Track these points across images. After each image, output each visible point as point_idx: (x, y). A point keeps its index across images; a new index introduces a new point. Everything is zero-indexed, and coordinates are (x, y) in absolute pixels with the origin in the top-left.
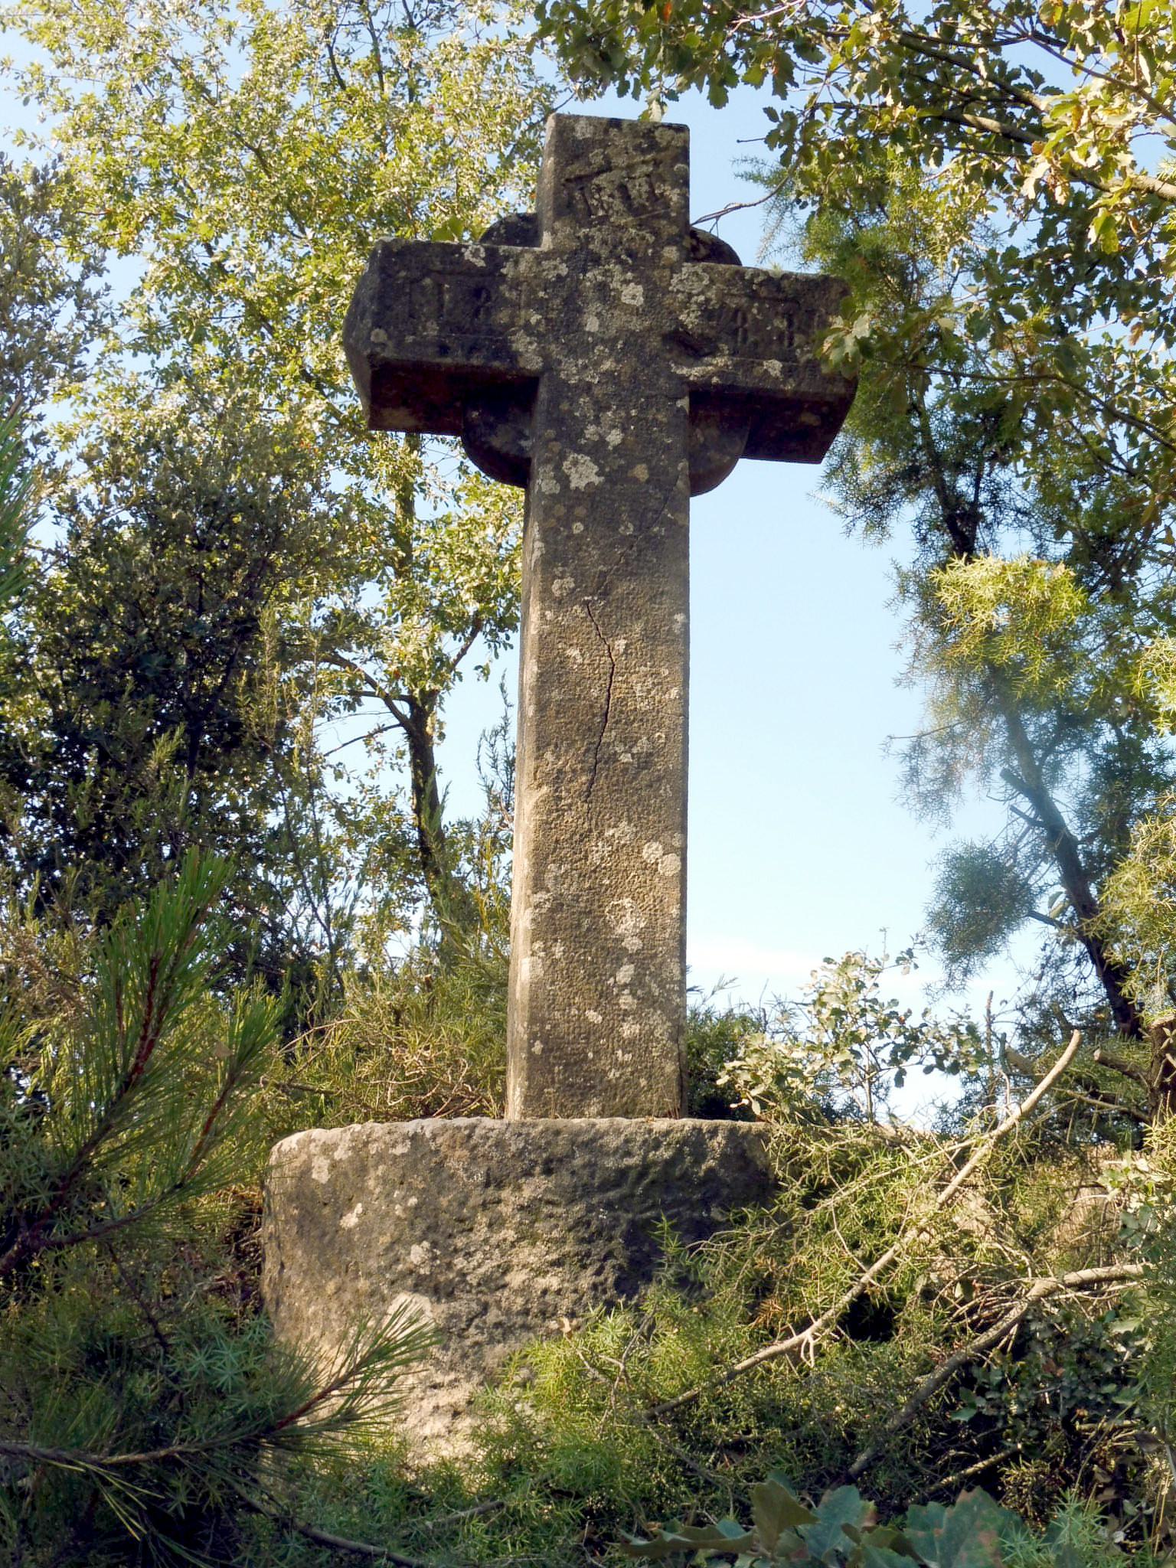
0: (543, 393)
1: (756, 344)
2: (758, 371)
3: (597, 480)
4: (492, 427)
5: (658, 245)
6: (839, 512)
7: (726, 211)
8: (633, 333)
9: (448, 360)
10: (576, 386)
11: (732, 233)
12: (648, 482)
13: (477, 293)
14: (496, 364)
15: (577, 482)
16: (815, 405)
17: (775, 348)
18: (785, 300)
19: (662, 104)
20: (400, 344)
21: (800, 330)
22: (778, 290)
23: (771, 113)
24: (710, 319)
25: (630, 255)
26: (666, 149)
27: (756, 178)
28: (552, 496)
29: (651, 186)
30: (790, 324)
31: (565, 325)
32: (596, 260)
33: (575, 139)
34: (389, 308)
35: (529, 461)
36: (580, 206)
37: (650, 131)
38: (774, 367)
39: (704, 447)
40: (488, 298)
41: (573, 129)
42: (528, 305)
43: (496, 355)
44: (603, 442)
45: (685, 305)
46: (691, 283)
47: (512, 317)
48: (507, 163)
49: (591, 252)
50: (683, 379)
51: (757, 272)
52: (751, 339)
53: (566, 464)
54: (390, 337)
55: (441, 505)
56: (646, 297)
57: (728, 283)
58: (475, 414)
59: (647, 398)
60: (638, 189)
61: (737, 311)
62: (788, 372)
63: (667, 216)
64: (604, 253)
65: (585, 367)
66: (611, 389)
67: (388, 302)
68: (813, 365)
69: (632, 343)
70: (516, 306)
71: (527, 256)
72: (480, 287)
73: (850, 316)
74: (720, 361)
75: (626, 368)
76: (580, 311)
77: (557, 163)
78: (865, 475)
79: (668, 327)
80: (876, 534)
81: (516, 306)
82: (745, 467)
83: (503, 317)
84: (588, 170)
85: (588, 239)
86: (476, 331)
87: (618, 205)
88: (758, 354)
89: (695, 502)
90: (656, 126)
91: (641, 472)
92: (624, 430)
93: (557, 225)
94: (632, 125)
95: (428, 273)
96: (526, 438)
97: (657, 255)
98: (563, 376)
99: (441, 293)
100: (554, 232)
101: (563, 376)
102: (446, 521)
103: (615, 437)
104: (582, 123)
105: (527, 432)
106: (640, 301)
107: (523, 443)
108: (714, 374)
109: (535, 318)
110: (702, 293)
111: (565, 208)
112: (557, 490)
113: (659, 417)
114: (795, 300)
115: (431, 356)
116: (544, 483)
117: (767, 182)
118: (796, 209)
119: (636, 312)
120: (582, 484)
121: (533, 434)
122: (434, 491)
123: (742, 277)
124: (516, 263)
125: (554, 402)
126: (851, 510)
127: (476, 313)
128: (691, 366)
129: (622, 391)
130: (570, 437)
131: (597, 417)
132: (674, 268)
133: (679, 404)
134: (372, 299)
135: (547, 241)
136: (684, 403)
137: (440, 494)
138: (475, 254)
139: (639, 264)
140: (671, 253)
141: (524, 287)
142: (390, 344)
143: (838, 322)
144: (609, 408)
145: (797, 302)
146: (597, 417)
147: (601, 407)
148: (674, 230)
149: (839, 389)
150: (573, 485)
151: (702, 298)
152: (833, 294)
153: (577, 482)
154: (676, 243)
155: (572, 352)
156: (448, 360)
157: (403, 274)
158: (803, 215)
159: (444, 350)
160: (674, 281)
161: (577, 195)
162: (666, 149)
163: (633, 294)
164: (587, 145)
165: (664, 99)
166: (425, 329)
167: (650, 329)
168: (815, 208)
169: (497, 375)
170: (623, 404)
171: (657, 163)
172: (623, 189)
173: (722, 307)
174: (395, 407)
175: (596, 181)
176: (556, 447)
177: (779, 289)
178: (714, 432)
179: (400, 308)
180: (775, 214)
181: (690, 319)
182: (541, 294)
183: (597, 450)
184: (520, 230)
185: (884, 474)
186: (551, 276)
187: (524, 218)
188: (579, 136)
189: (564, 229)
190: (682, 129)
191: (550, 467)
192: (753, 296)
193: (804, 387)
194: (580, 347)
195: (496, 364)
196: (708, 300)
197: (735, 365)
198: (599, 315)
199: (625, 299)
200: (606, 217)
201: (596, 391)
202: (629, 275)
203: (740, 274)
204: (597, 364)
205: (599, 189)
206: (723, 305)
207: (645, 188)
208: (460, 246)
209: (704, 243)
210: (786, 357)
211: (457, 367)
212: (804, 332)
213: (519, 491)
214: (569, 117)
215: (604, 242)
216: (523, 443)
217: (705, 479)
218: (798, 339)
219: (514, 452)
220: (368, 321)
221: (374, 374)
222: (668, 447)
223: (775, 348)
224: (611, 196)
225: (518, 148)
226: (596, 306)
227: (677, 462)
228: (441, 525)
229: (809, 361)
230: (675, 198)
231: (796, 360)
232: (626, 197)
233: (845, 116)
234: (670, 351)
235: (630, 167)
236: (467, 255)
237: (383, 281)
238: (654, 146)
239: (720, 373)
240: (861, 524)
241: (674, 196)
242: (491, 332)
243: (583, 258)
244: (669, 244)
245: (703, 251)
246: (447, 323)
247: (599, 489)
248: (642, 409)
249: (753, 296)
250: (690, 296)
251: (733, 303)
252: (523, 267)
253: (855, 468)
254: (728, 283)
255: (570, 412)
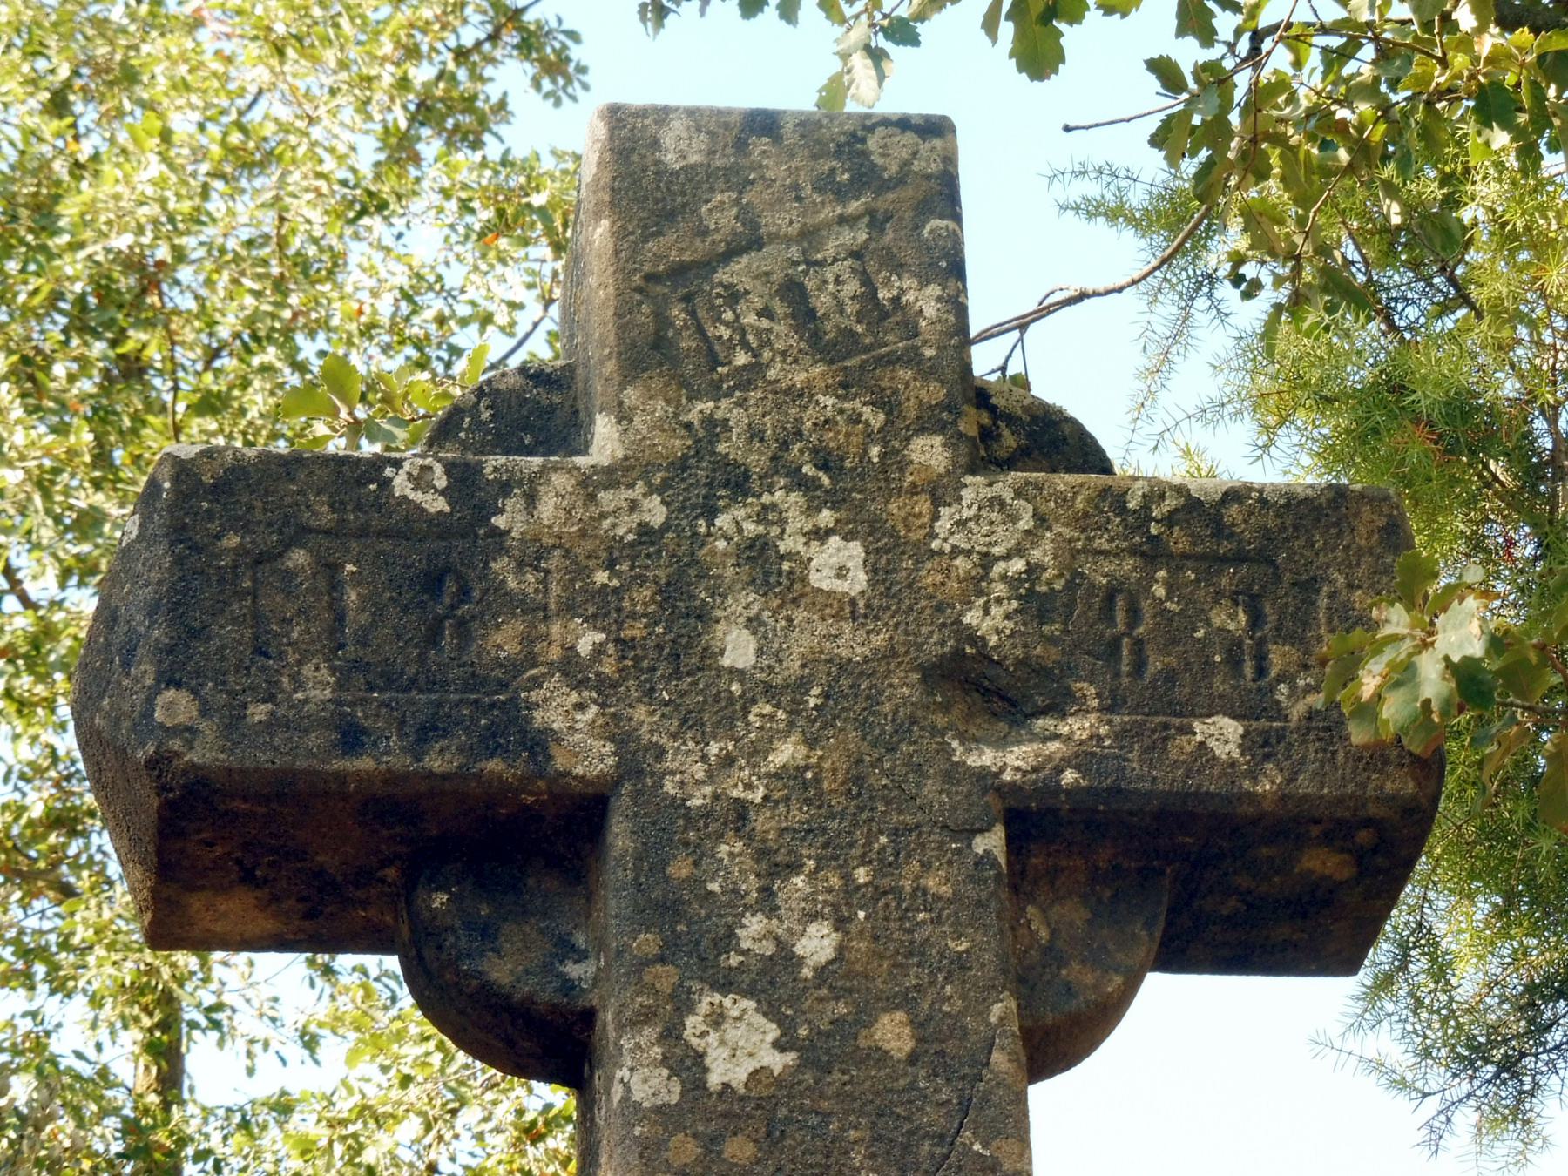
0: (621, 836)
1: (1170, 676)
2: (1182, 746)
3: (778, 1062)
4: (487, 933)
5: (897, 431)
6: (1402, 1084)
7: (1043, 311)
8: (844, 666)
9: (365, 763)
10: (707, 813)
11: (1074, 372)
12: (913, 1059)
13: (433, 582)
14: (494, 765)
15: (724, 1070)
16: (1338, 827)
17: (1220, 685)
18: (1239, 558)
19: (877, 56)
20: (233, 724)
21: (1281, 635)
22: (1214, 532)
23: (1164, 71)
24: (1043, 617)
25: (824, 467)
26: (900, 181)
27: (1116, 213)
28: (659, 1110)
29: (867, 281)
30: (1256, 620)
31: (668, 652)
32: (739, 484)
33: (661, 171)
34: (195, 634)
35: (588, 1017)
36: (687, 343)
37: (854, 138)
38: (1223, 734)
39: (1053, 955)
40: (464, 593)
41: (655, 144)
42: (569, 609)
43: (491, 743)
44: (785, 957)
45: (977, 584)
46: (988, 529)
47: (528, 640)
48: (400, 150)
49: (724, 463)
50: (985, 779)
51: (1157, 491)
52: (1155, 664)
53: (694, 1024)
54: (204, 712)
55: (265, 1061)
56: (873, 570)
57: (1082, 521)
58: (440, 899)
59: (895, 833)
60: (834, 292)
61: (1110, 595)
62: (1260, 746)
63: (911, 357)
64: (757, 461)
65: (728, 761)
66: (797, 815)
67: (196, 618)
68: (1326, 726)
69: (843, 692)
70: (536, 611)
71: (560, 480)
72: (442, 566)
73: (1430, 611)
74: (1079, 727)
75: (834, 759)
76: (703, 616)
77: (619, 234)
78: (1468, 982)
79: (935, 645)
80: (1507, 1143)
81: (536, 611)
82: (1160, 992)
83: (505, 640)
84: (701, 248)
85: (715, 428)
86: (432, 685)
87: (783, 334)
88: (1175, 704)
89: (1041, 1095)
90: (870, 123)
91: (892, 1033)
92: (840, 923)
93: (632, 395)
94: (806, 124)
95: (300, 535)
96: (582, 956)
97: (895, 460)
98: (670, 787)
99: (335, 586)
100: (624, 416)
101: (670, 787)
102: (283, 1107)
103: (817, 945)
104: (678, 126)
105: (580, 940)
106: (857, 581)
107: (573, 970)
108: (1066, 762)
109: (587, 641)
110: (1018, 551)
111: (647, 355)
112: (673, 1094)
113: (931, 883)
114: (1263, 557)
115: (313, 752)
116: (637, 1077)
117: (1143, 222)
118: (1227, 293)
119: (848, 610)
120: (738, 1076)
121: (601, 946)
122: (247, 1023)
123: (1120, 506)
124: (531, 499)
125: (652, 858)
126: (1436, 1077)
127: (433, 638)
128: (1002, 743)
129: (831, 822)
130: (698, 950)
131: (767, 892)
132: (940, 492)
133: (981, 844)
134: (152, 611)
135: (606, 441)
136: (992, 842)
137: (262, 1030)
138: (420, 479)
139: (849, 487)
140: (930, 453)
141: (555, 560)
142: (208, 728)
143: (1396, 619)
144: (794, 867)
145: (1264, 566)
146: (767, 892)
147: (775, 866)
148: (935, 392)
149: (1401, 784)
150: (714, 1080)
151: (1018, 565)
152: (1364, 530)
153: (724, 1070)
154: (939, 428)
155: (690, 723)
156: (365, 763)
157: (232, 540)
158: (1251, 314)
159: (352, 738)
160: (942, 526)
161: (677, 313)
162: (900, 181)
163: (839, 566)
164: (697, 181)
165: (881, 41)
166: (299, 685)
167: (890, 653)
168: (1283, 295)
169: (497, 792)
170: (833, 854)
171: (878, 223)
172: (793, 291)
173: (1070, 587)
174: (223, 889)
175: (722, 276)
176: (665, 977)
177: (1220, 530)
178: (1074, 914)
179: (227, 633)
180: (1168, 308)
181: (990, 621)
182: (601, 577)
183: (773, 981)
184: (531, 412)
185: (1515, 983)
186: (624, 528)
187: (534, 375)
188: (671, 159)
189: (650, 405)
190: (936, 128)
191: (649, 1033)
192: (1152, 553)
193: (1305, 784)
194: (713, 709)
195: (494, 765)
196: (1033, 570)
197: (1120, 735)
198: (753, 624)
199: (821, 579)
200: (757, 368)
201: (761, 823)
202: (826, 517)
203: (1114, 497)
204: (758, 752)
205: (734, 296)
206: (1075, 581)
207: (852, 287)
208: (378, 463)
209: (1010, 419)
210: (1254, 708)
211: (391, 778)
212: (1294, 639)
213: (558, 1097)
214: (642, 113)
215: (755, 434)
216: (573, 970)
217: (1058, 1041)
218: (1279, 657)
219: (547, 994)
220: (145, 671)
221: (168, 806)
222: (961, 963)
223: (1220, 685)
224: (765, 313)
225: (425, 112)
226: (745, 602)
227: (986, 1004)
228: (264, 1115)
229: (1311, 715)
230: (930, 310)
231: (1279, 713)
232: (804, 316)
233: (1345, 54)
234: (946, 708)
235: (809, 236)
236: (401, 484)
237: (179, 561)
238: (866, 177)
239: (1082, 759)
240: (1466, 1117)
241: (927, 302)
242: (475, 682)
243: (702, 477)
244: (922, 430)
245: (1009, 441)
246: (357, 665)
247: (784, 1084)
248: (885, 866)
249: (1152, 553)
250: (987, 561)
251: (1100, 573)
252: (547, 509)
253: (1440, 971)
254: (1082, 521)
255: (697, 883)
